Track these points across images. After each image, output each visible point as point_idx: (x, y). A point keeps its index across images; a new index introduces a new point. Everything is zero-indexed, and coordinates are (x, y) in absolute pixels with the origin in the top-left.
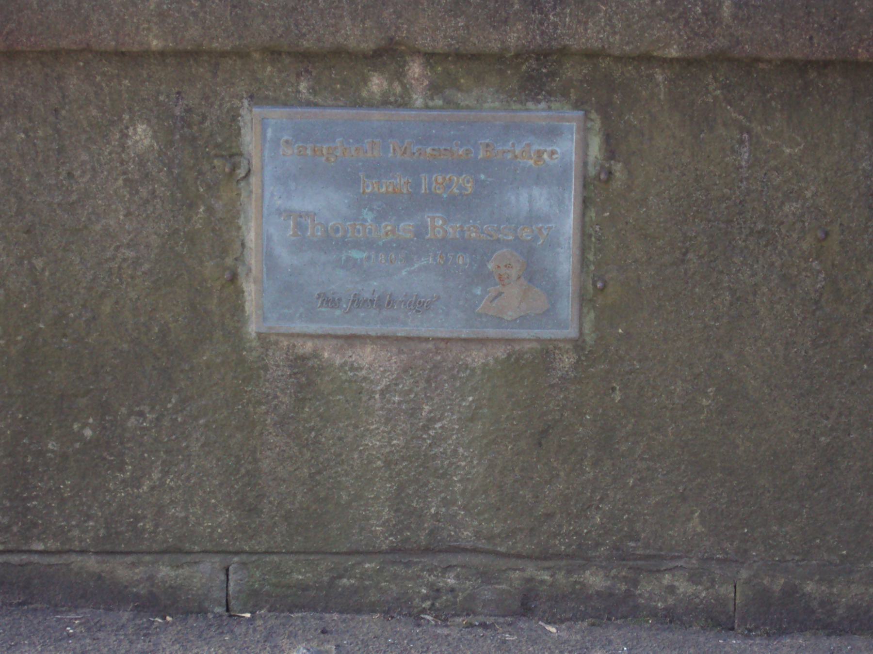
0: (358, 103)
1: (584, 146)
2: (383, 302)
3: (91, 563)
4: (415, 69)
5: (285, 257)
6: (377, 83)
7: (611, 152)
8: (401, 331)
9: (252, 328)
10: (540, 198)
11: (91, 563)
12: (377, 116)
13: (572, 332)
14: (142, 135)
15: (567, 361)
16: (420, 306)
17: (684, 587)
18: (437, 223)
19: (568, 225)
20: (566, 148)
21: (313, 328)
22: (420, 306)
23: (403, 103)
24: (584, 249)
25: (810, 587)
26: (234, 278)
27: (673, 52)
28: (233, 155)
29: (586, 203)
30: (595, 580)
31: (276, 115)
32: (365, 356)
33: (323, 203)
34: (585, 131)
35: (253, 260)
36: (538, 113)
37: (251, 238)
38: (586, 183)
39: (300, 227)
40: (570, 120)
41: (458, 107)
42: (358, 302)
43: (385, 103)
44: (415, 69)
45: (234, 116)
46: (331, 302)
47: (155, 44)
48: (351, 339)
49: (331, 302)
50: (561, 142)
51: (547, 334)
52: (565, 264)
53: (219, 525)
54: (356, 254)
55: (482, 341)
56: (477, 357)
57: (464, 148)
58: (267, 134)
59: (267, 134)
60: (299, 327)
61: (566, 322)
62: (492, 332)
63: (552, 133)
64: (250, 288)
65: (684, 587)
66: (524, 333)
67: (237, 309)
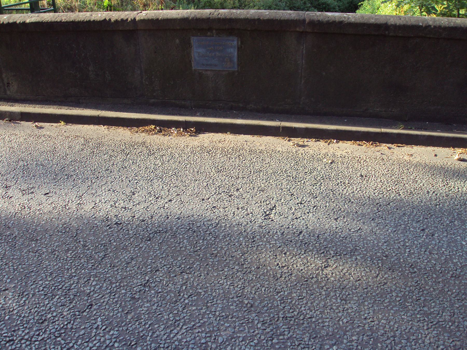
0: (207, 36)
1: (238, 43)
2: (211, 65)
3: (173, 101)
4: (214, 31)
5: (197, 58)
6: (209, 33)
7: (242, 43)
8: (213, 69)
9: (193, 68)
10: (232, 50)
11: (173, 101)
12: (209, 38)
13: (237, 70)
14: (177, 41)
15: (237, 74)
16: (216, 66)
17: (253, 106)
18: (218, 54)
19: (236, 54)
20: (235, 43)
21: (201, 69)
22: (216, 66)
23: (213, 36)
24: (238, 58)
25: (270, 107)
26: (190, 61)
27: (249, 29)
28: (190, 44)
29: (238, 51)
30: (241, 105)
31: (195, 38)
32: (209, 73)
33: (201, 51)
34: (238, 41)
35: (193, 59)
36: (231, 38)
37: (192, 56)
38: (238, 48)
39: (199, 54)
40: (236, 39)
41: (220, 37)
42: (207, 65)
43: (210, 36)
44: (214, 31)
45: (190, 38)
46: (203, 65)
47: (178, 28)
48: (206, 70)
49: (203, 65)
50: (234, 42)
51: (233, 70)
52: (236, 60)
53: (15, 283)
54: (207, 58)
55: (225, 71)
56: (224, 73)
57: (417, 271)
58: (194, 40)
59: (194, 40)
60: (199, 68)
61: (236, 68)
62: (225, 69)
63: (233, 41)
64: (193, 63)
65: (253, 106)
66: (230, 70)
67: (191, 66)
